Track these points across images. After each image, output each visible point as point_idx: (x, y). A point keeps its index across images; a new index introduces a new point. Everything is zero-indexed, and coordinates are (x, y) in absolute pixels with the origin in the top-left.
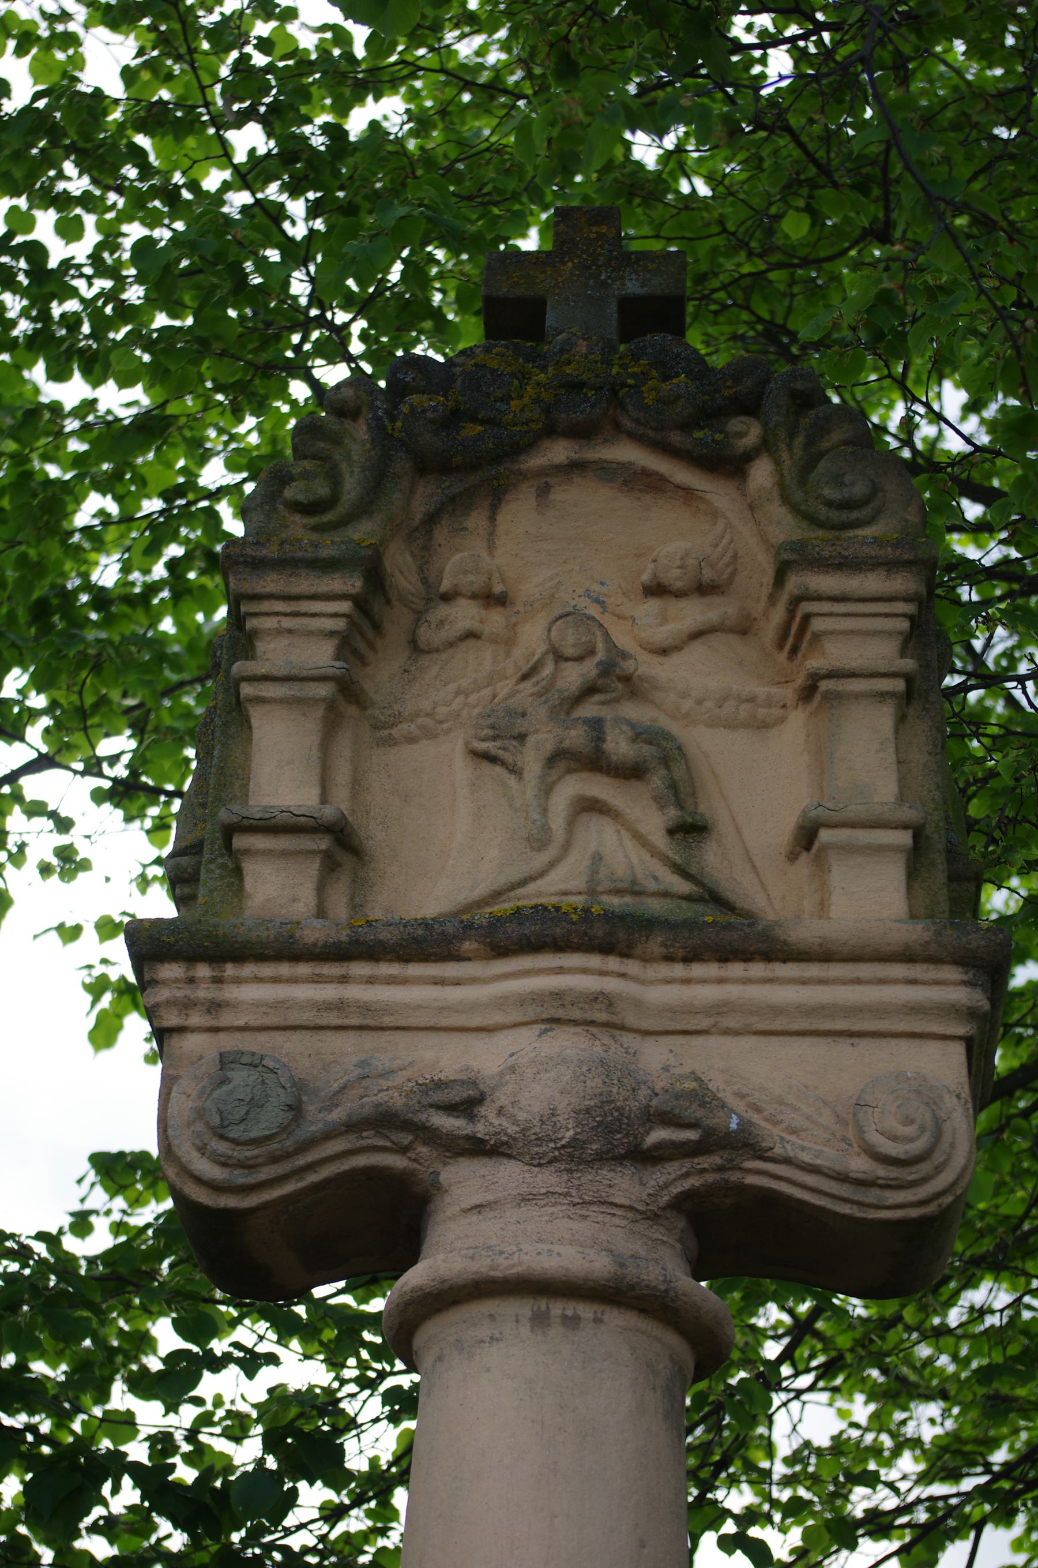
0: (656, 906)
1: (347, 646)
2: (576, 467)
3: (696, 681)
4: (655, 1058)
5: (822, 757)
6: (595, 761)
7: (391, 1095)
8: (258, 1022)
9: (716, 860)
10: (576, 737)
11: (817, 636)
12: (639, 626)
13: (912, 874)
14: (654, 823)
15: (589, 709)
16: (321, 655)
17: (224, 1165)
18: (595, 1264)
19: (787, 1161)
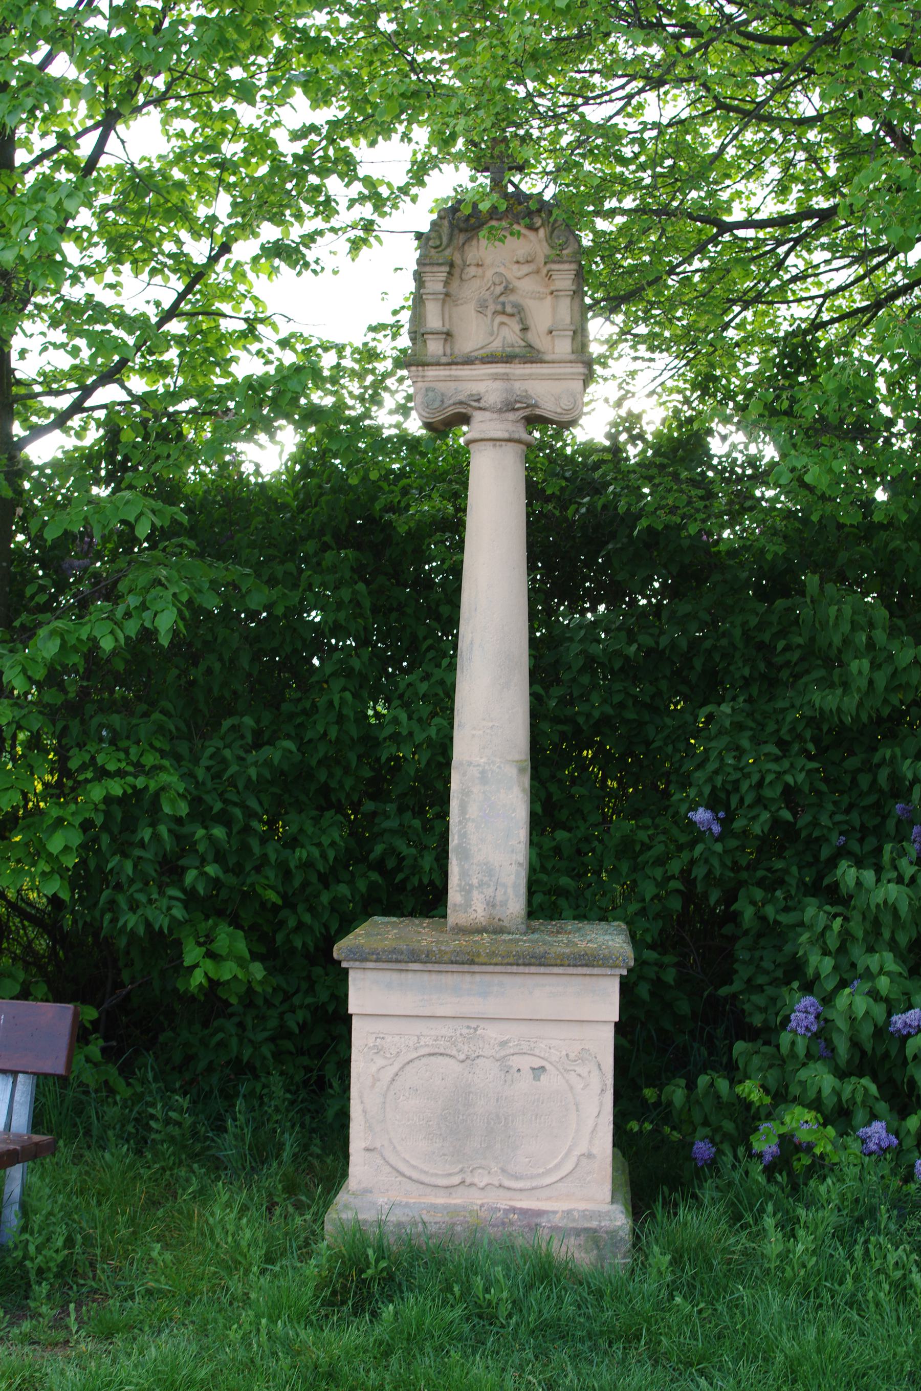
0: (517, 350)
1: (446, 283)
3: (527, 287)
4: (518, 386)
5: (554, 309)
6: (504, 313)
7: (462, 397)
9: (531, 337)
10: (499, 308)
12: (513, 272)
13: (573, 339)
14: (517, 328)
15: (502, 299)
16: (439, 287)
18: (506, 435)
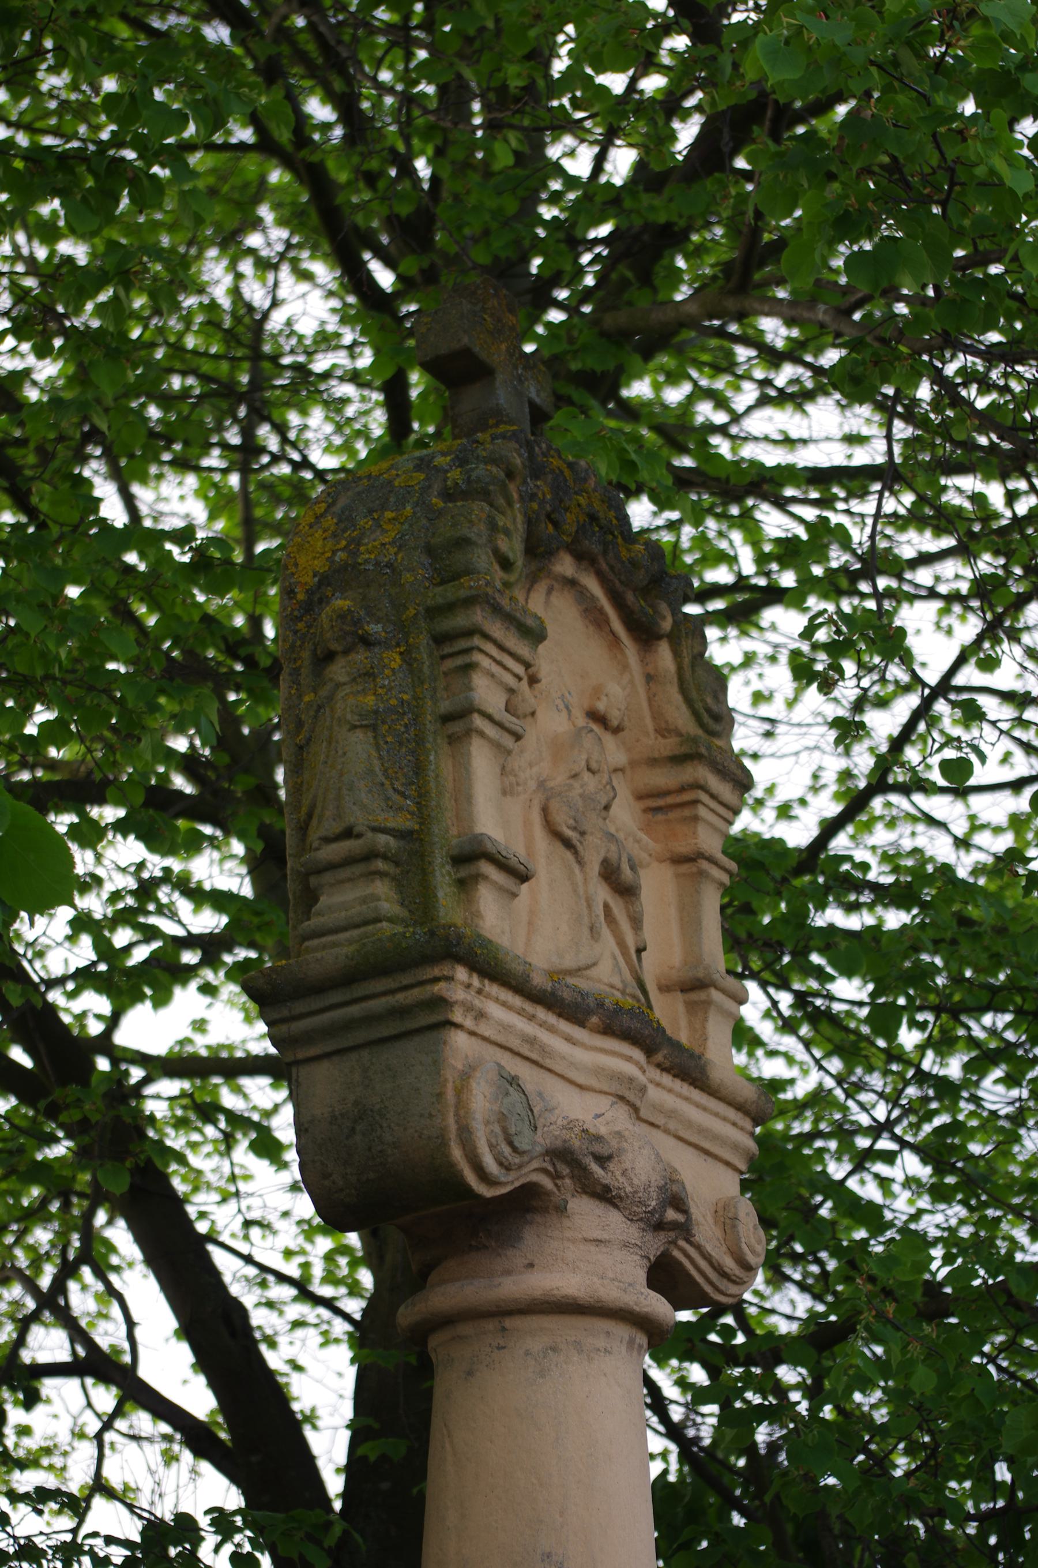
2: (572, 583)
8: (493, 1038)
11: (696, 818)
17: (501, 1164)
19: (698, 1248)
